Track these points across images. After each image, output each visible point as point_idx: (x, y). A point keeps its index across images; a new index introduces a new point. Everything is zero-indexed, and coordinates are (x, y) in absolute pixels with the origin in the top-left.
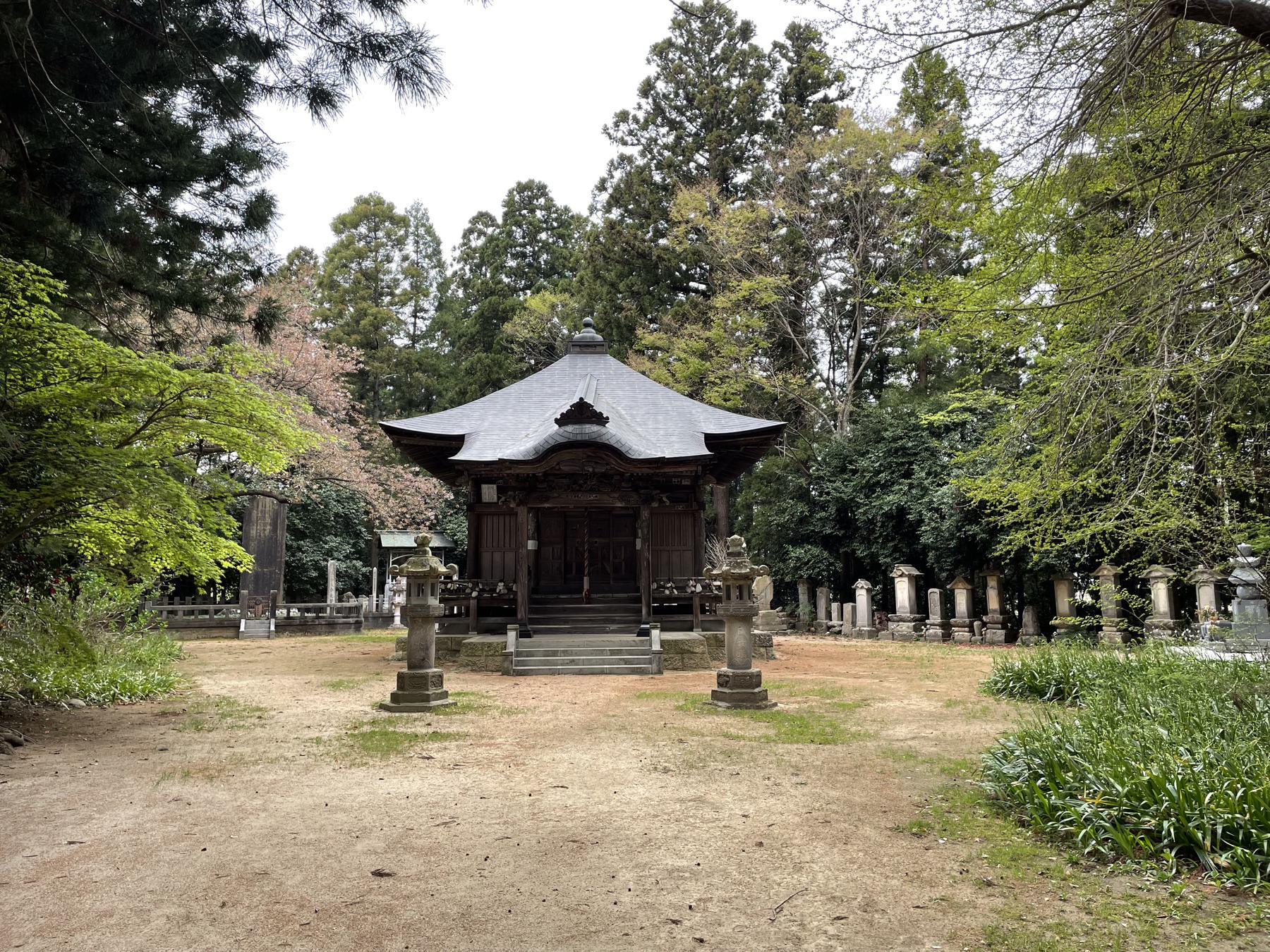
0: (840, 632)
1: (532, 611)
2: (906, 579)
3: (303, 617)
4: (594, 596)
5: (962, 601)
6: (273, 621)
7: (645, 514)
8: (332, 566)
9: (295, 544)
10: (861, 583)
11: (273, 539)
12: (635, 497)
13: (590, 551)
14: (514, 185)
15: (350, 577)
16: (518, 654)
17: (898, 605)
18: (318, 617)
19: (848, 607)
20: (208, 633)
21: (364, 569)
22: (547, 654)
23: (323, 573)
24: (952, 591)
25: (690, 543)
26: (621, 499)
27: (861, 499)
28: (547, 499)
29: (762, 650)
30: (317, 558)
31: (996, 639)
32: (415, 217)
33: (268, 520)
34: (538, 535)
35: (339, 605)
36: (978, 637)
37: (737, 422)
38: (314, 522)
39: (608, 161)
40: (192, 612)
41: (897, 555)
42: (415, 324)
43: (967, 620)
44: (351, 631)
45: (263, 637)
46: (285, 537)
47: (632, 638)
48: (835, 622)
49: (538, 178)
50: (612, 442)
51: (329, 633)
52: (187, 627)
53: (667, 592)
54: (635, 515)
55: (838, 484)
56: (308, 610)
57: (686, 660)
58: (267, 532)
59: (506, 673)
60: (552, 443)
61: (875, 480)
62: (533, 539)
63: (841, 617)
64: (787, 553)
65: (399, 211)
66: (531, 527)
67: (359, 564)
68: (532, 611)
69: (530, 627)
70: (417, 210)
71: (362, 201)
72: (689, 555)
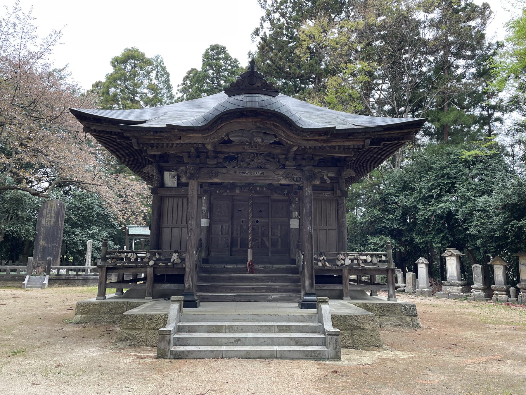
0: (404, 291)
2: (454, 258)
3: (67, 274)
4: (256, 266)
5: (499, 273)
6: (47, 277)
7: (308, 190)
9: (71, 230)
11: (55, 227)
12: (299, 174)
13: (253, 229)
14: (209, 47)
16: (179, 329)
17: (448, 275)
20: (5, 284)
22: (211, 330)
23: (85, 246)
24: (492, 267)
26: (286, 177)
28: (217, 175)
29: (408, 319)
32: (156, 62)
33: (53, 215)
34: (210, 214)
36: (513, 298)
38: (84, 218)
39: (260, 17)
41: (445, 242)
43: (505, 287)
45: (38, 287)
46: (63, 226)
47: (292, 309)
48: (400, 284)
49: (221, 44)
50: (283, 111)
51: (83, 285)
53: (320, 264)
55: (402, 197)
56: (72, 270)
58: (52, 222)
60: (222, 110)
62: (206, 217)
63: (405, 282)
64: (367, 240)
65: (148, 56)
66: (204, 207)
68: (201, 279)
70: (158, 58)
71: (128, 50)
72: (333, 233)
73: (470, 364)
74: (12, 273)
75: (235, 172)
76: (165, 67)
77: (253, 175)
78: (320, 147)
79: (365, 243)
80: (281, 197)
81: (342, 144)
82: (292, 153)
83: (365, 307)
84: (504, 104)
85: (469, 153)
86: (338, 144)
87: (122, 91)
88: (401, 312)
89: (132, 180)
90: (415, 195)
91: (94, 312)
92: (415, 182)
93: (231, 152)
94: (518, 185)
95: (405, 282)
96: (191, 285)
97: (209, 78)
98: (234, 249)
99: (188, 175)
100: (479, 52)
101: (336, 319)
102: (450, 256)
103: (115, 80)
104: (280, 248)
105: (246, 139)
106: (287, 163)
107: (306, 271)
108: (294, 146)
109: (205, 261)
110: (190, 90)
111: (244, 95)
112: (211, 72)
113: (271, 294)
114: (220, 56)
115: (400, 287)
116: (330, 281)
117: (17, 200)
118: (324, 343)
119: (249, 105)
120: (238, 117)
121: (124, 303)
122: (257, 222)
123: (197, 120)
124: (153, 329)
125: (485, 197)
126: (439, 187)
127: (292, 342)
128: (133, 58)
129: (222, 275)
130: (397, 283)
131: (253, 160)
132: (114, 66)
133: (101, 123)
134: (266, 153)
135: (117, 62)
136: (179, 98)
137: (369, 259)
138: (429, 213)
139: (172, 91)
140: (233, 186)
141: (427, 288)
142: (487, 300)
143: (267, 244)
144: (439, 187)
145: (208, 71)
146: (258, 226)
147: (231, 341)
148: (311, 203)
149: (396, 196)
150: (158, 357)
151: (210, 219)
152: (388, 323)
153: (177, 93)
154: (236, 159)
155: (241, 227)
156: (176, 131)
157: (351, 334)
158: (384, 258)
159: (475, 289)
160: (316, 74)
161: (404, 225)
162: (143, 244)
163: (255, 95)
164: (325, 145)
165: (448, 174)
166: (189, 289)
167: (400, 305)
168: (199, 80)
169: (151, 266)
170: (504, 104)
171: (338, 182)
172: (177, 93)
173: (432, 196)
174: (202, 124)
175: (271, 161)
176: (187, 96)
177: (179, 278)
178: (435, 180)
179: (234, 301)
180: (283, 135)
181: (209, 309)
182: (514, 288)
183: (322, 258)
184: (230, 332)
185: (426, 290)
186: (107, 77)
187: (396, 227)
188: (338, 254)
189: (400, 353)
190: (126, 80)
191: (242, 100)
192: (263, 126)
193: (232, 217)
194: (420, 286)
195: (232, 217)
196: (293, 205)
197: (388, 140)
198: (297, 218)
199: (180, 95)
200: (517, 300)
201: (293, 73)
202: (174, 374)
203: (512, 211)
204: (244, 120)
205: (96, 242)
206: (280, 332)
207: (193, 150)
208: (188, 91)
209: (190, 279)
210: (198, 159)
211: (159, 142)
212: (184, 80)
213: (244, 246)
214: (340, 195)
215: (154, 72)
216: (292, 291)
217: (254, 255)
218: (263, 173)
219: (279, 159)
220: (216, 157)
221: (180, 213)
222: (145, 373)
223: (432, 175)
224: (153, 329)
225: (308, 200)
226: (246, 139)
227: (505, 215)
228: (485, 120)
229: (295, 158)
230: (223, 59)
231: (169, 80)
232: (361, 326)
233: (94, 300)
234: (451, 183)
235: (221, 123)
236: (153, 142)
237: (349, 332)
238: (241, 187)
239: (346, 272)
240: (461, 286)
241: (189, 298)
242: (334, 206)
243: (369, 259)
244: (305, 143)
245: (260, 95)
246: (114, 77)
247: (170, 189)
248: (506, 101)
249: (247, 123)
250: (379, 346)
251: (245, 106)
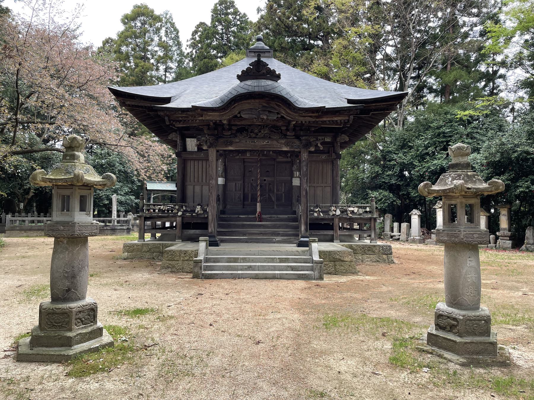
0: (398, 239)
1: (220, 226)
4: (264, 216)
7: (304, 156)
8: (114, 197)
10: (415, 211)
12: (297, 142)
13: (261, 186)
15: (128, 204)
16: (207, 260)
18: (106, 226)
19: (404, 225)
21: (136, 201)
22: (229, 260)
23: (111, 200)
25: (329, 181)
26: (287, 145)
27: (416, 163)
28: (231, 144)
29: (385, 256)
30: (108, 194)
31: (505, 246)
32: (166, 18)
35: (118, 219)
37: (369, 93)
40: (33, 222)
42: (165, 75)
44: (125, 233)
47: (293, 248)
48: (396, 233)
50: (283, 94)
51: (112, 234)
52: (31, 229)
53: (316, 214)
54: (297, 155)
57: (338, 267)
59: (196, 276)
60: (235, 93)
61: (425, 151)
62: (222, 177)
63: (400, 231)
64: (367, 194)
65: (157, 13)
66: (220, 169)
67: (133, 198)
68: (220, 226)
69: (218, 238)
70: (167, 14)
71: (136, 7)
72: (328, 190)
73: (416, 283)
74: (39, 224)
75: (246, 141)
76: (174, 23)
77: (261, 144)
78: (314, 122)
79: (365, 198)
80: (285, 160)
81: (331, 119)
82: (292, 126)
83: (351, 247)
84: (509, 60)
85: (463, 113)
86: (328, 119)
87: (134, 49)
88: (380, 251)
89: (153, 141)
90: (413, 152)
91: (138, 251)
92: (413, 141)
93: (242, 125)
94: (501, 145)
95: (400, 232)
96: (213, 230)
97: (218, 34)
98: (246, 203)
99: (208, 144)
100: (484, 10)
101: (322, 253)
103: (126, 37)
104: (283, 201)
105: (254, 116)
106: (288, 133)
107: (302, 220)
108: (293, 121)
109: (223, 212)
110: (200, 45)
111: (253, 81)
112: (220, 27)
113: (275, 237)
114: (229, 11)
116: (322, 228)
117: (46, 159)
118: (312, 269)
119: (256, 89)
120: (247, 98)
121: (160, 244)
122: (265, 180)
123: (215, 101)
124: (187, 260)
125: (475, 155)
126: (435, 145)
127: (289, 269)
128: (143, 15)
129: (236, 223)
130: (393, 232)
131: (260, 132)
132: (125, 23)
133: (135, 99)
134: (270, 125)
135: (127, 19)
136: (188, 54)
137: (356, 210)
138: (424, 170)
139: (182, 48)
140: (244, 152)
141: (419, 236)
143: (273, 199)
144: (435, 145)
145: (217, 26)
146: (266, 184)
147: (245, 268)
148: (307, 166)
149: (395, 154)
150: (193, 278)
151: (225, 178)
152: (369, 260)
153: (186, 49)
154: (247, 130)
155: (252, 185)
156: (199, 110)
157: (332, 264)
158: (368, 209)
160: (324, 33)
161: (401, 180)
162: (160, 198)
163: (261, 81)
164: (317, 120)
165: (444, 133)
166: (211, 233)
167: (379, 245)
168: (208, 36)
169: (180, 216)
170: (509, 60)
171: (334, 147)
172: (186, 49)
173: (427, 154)
174: (220, 105)
175: (275, 132)
176: (196, 52)
177: (203, 225)
178: (431, 138)
179: (246, 242)
180: (283, 112)
181: (227, 247)
183: (317, 210)
184: (244, 262)
185: (417, 238)
186: (118, 36)
187: (394, 182)
188: (331, 206)
189: (369, 277)
190: (136, 37)
191: (251, 85)
192: (267, 106)
193: (244, 176)
194: (412, 234)
195: (244, 176)
196: (295, 166)
197: (375, 110)
198: (298, 177)
199: (189, 50)
201: (301, 32)
202: (207, 286)
203: (495, 168)
204: (253, 101)
205: (119, 197)
206: (280, 262)
207: (211, 124)
208: (197, 45)
209: (212, 225)
210: (216, 131)
211: (186, 119)
212: (193, 35)
213: (254, 200)
214: (335, 157)
215: (164, 29)
216: (293, 236)
217: (262, 208)
218: (268, 142)
219: (281, 130)
220: (230, 129)
221: (200, 173)
222: (187, 285)
223: (429, 134)
224: (187, 260)
225: (304, 163)
226: (254, 116)
227: (489, 171)
228: (490, 77)
229: (294, 130)
230: (232, 14)
231: (178, 37)
232: (342, 259)
233: (136, 242)
235: (235, 104)
236: (181, 119)
237: (332, 263)
238: (250, 151)
239: (336, 220)
241: (212, 239)
242: (330, 166)
243: (356, 210)
244: (302, 119)
245: (265, 80)
246: (125, 36)
247: (192, 153)
248: (511, 56)
249: (255, 103)
250: (355, 273)
251: (253, 90)
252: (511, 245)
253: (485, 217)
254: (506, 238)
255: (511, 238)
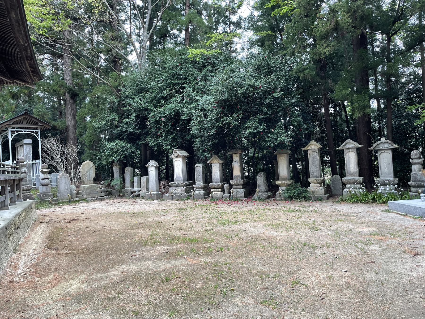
0: (139, 195)
2: (180, 159)
17: (175, 176)
31: (239, 195)
36: (227, 195)
41: (174, 144)
43: (220, 184)
48: (136, 189)
95: (140, 187)
102: (177, 157)
115: (135, 192)
141: (157, 191)
142: (205, 198)
144: (170, 87)
149: (132, 99)
159: (196, 188)
182: (228, 185)
185: (154, 193)
200: (230, 196)
234: (180, 84)
240: (186, 186)
252: (244, 194)
253: (218, 165)
254: (239, 187)
255: (244, 186)
